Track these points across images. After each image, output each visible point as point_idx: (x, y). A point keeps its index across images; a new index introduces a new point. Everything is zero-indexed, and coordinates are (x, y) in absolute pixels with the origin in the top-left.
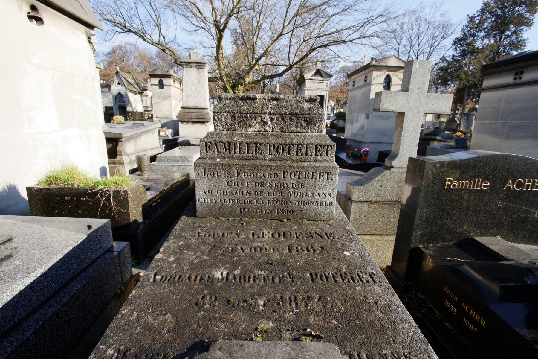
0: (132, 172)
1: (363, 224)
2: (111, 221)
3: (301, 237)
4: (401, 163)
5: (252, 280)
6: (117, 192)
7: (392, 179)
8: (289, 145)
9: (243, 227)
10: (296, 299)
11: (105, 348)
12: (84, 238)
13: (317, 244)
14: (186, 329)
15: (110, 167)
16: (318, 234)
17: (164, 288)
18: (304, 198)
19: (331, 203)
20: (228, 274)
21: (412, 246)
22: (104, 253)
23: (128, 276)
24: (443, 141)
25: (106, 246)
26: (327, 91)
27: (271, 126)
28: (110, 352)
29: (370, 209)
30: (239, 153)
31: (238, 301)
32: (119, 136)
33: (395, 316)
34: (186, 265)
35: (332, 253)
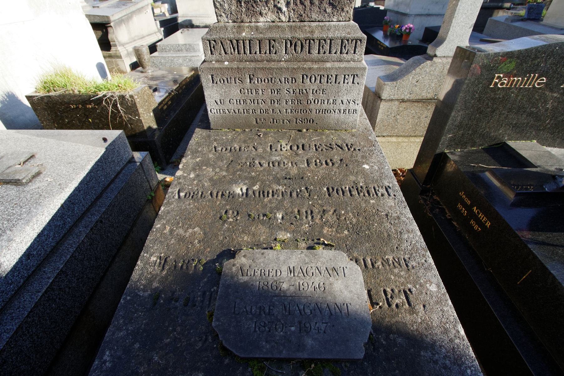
0: (134, 66)
1: (391, 125)
2: (125, 130)
3: (320, 149)
4: (445, 51)
5: (270, 195)
6: (122, 97)
7: (432, 73)
8: (310, 40)
9: (260, 140)
10: (312, 212)
11: (148, 256)
12: (103, 152)
13: (336, 157)
14: (214, 240)
15: (106, 62)
16: (338, 146)
17: (189, 204)
18: (325, 106)
19: (355, 111)
20: (247, 190)
21: (438, 151)
22: (127, 164)
23: (155, 183)
24: (513, 8)
25: (126, 157)
27: (287, 14)
28: (153, 259)
29: (401, 109)
30: (250, 53)
31: (259, 215)
32: (106, 20)
33: (403, 227)
34: (206, 182)
35: (351, 166)
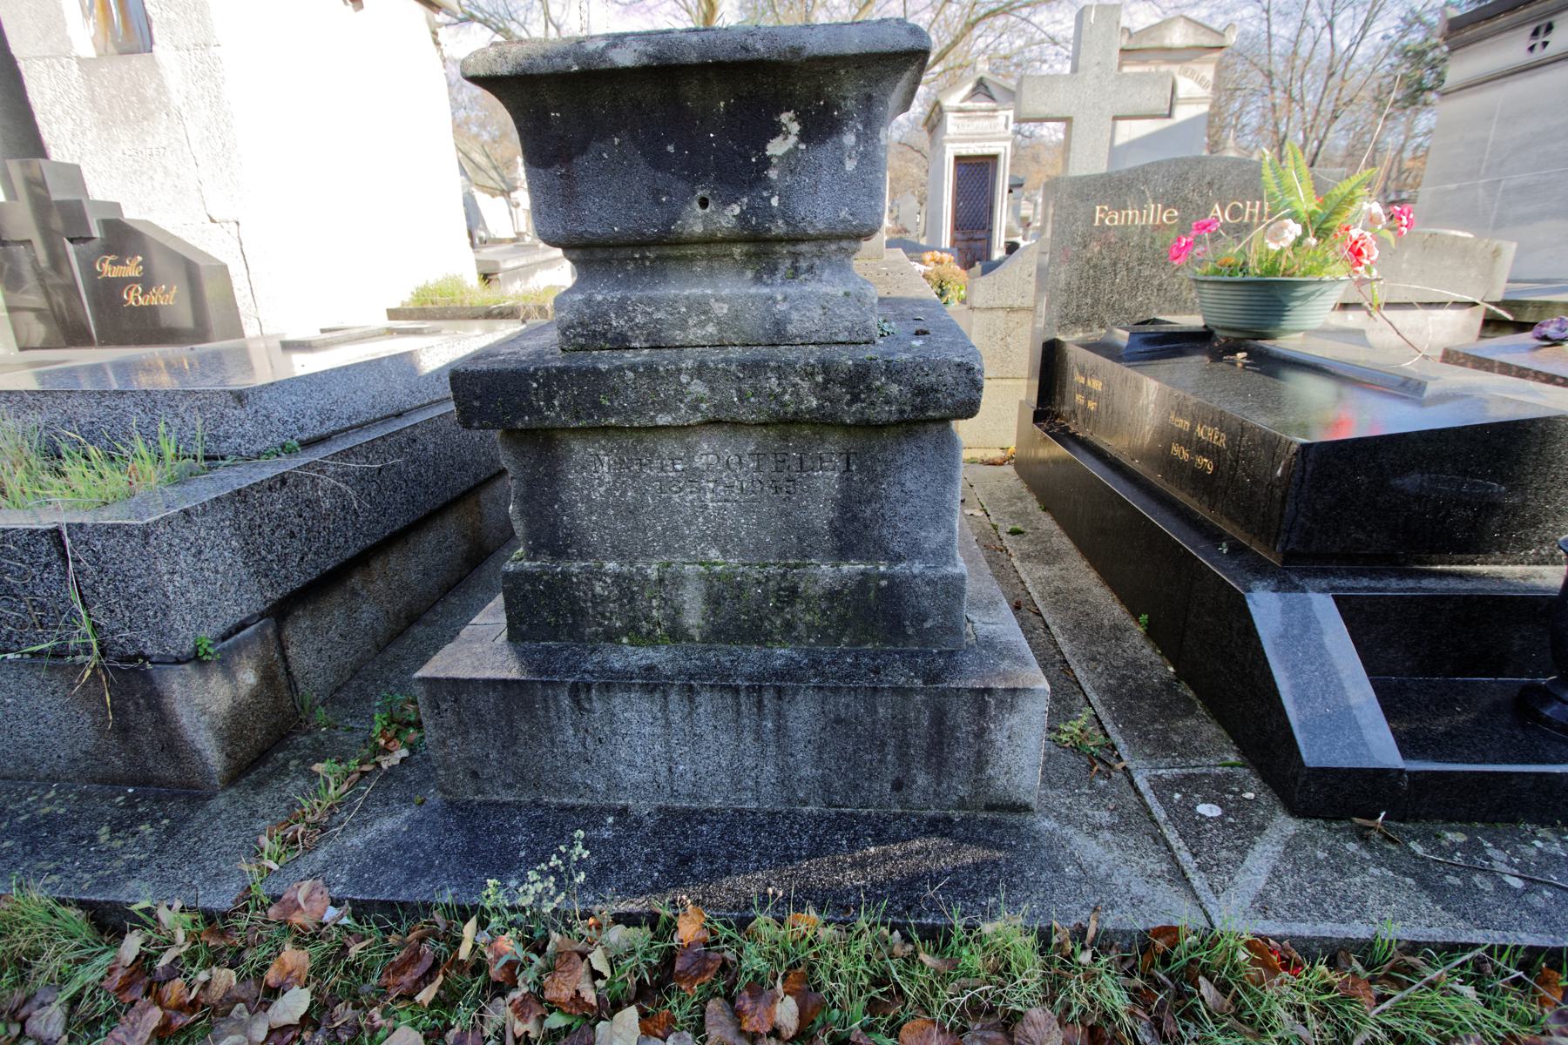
26: (1006, 139)
